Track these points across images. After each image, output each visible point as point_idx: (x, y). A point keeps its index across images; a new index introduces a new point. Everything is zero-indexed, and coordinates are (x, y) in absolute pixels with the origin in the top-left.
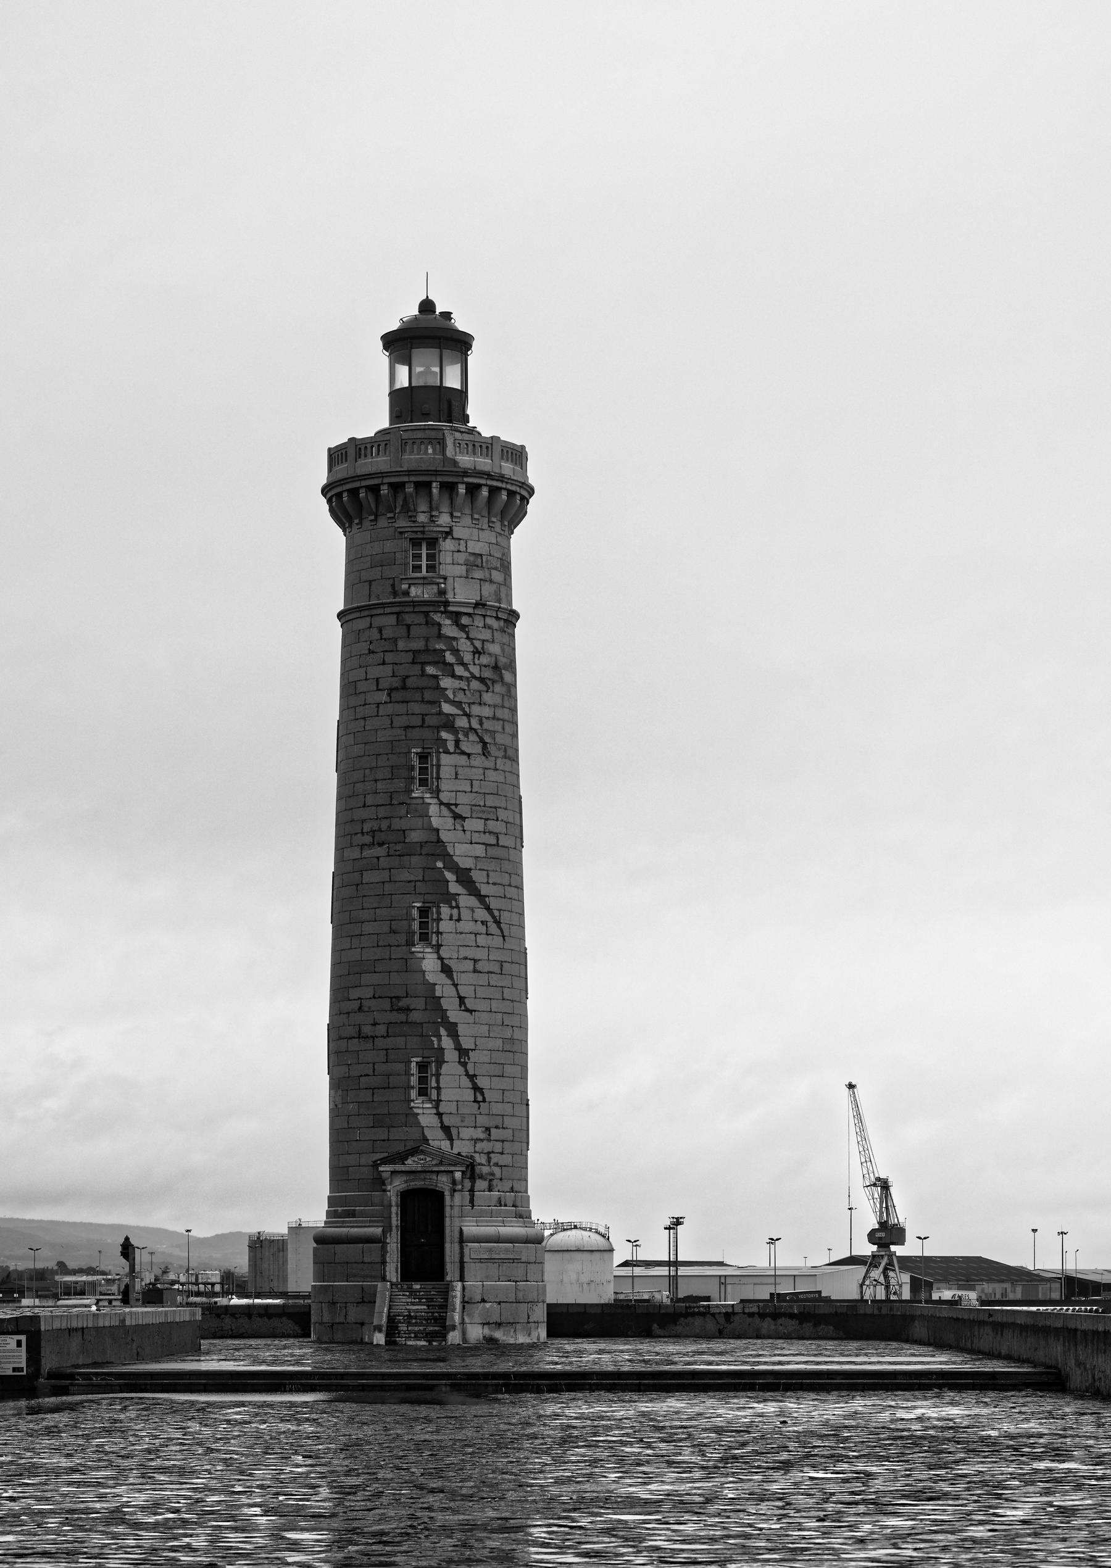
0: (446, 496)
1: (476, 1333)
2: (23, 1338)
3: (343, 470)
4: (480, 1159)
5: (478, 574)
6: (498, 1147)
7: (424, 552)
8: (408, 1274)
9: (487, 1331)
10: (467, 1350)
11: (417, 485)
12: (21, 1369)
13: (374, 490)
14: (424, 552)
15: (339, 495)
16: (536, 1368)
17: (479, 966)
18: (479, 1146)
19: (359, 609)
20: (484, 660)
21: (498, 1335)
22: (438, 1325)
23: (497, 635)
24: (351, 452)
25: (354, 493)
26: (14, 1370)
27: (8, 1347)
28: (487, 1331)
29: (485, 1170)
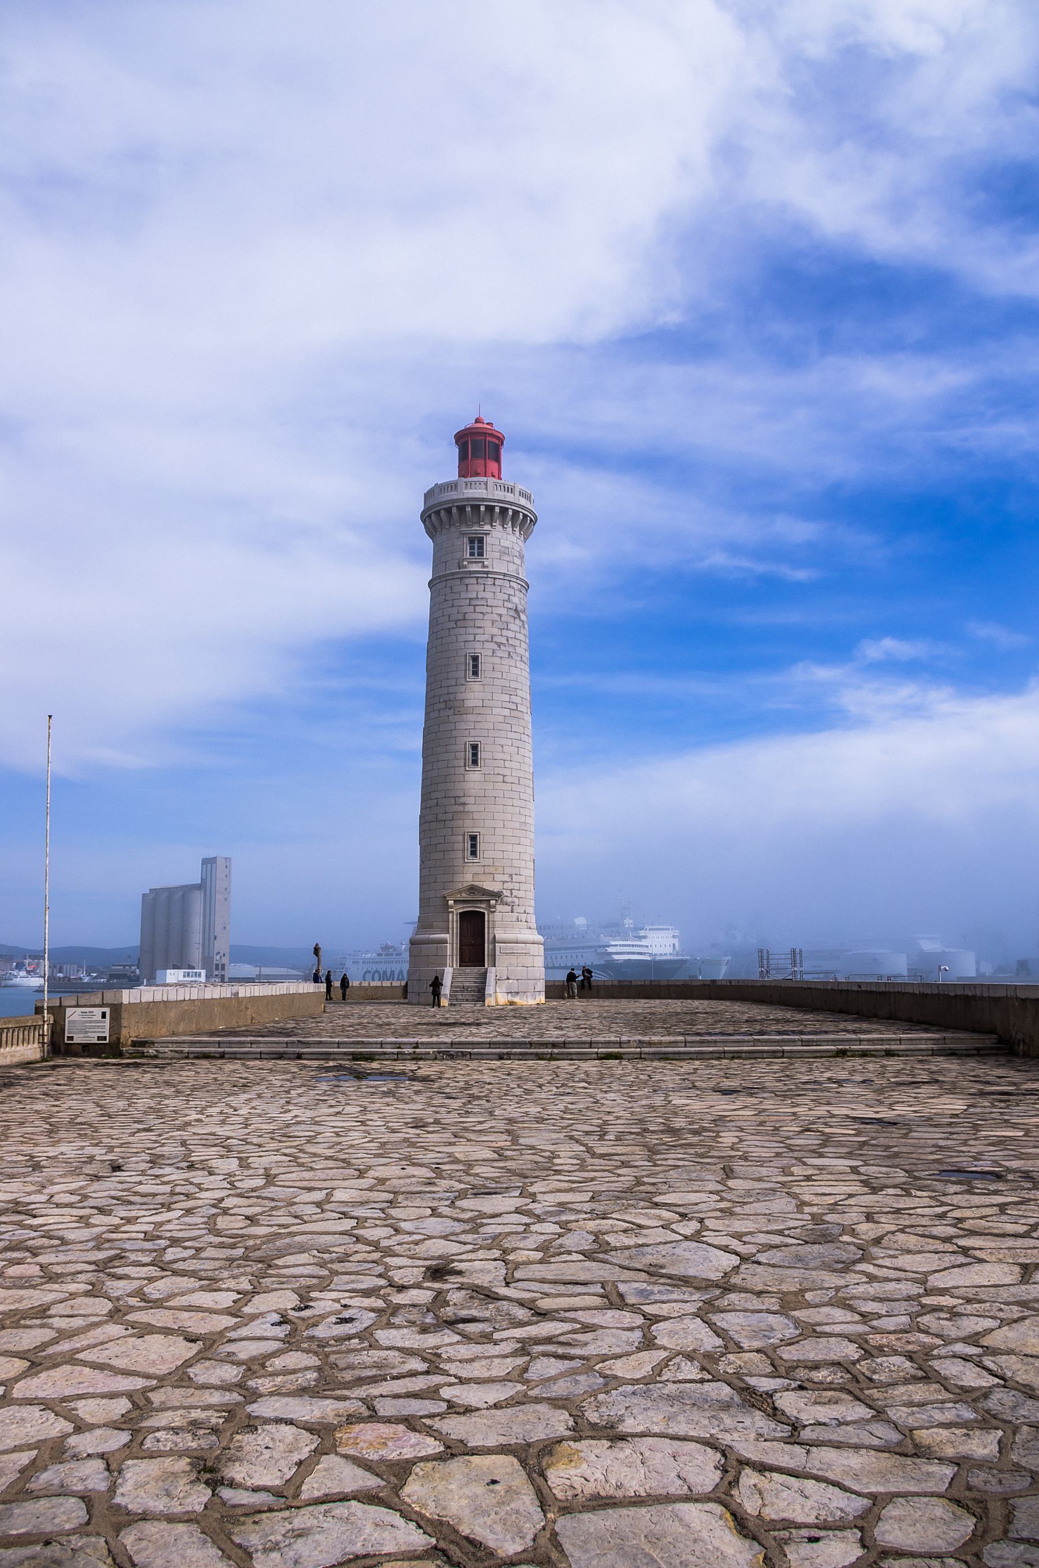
0: (489, 514)
1: (503, 999)
2: (107, 1010)
3: (431, 502)
4: (506, 893)
5: (506, 558)
6: (517, 886)
7: (476, 545)
8: (464, 962)
9: (510, 998)
10: (501, 1015)
11: (472, 506)
12: (105, 1038)
13: (449, 511)
14: (476, 545)
15: (430, 516)
16: (976, 1036)
17: (506, 779)
18: (506, 885)
19: (440, 577)
20: (510, 605)
21: (516, 999)
22: (480, 994)
23: (517, 593)
24: (437, 491)
25: (438, 513)
26: (99, 1038)
27: (95, 1018)
28: (510, 998)
29: (509, 900)
